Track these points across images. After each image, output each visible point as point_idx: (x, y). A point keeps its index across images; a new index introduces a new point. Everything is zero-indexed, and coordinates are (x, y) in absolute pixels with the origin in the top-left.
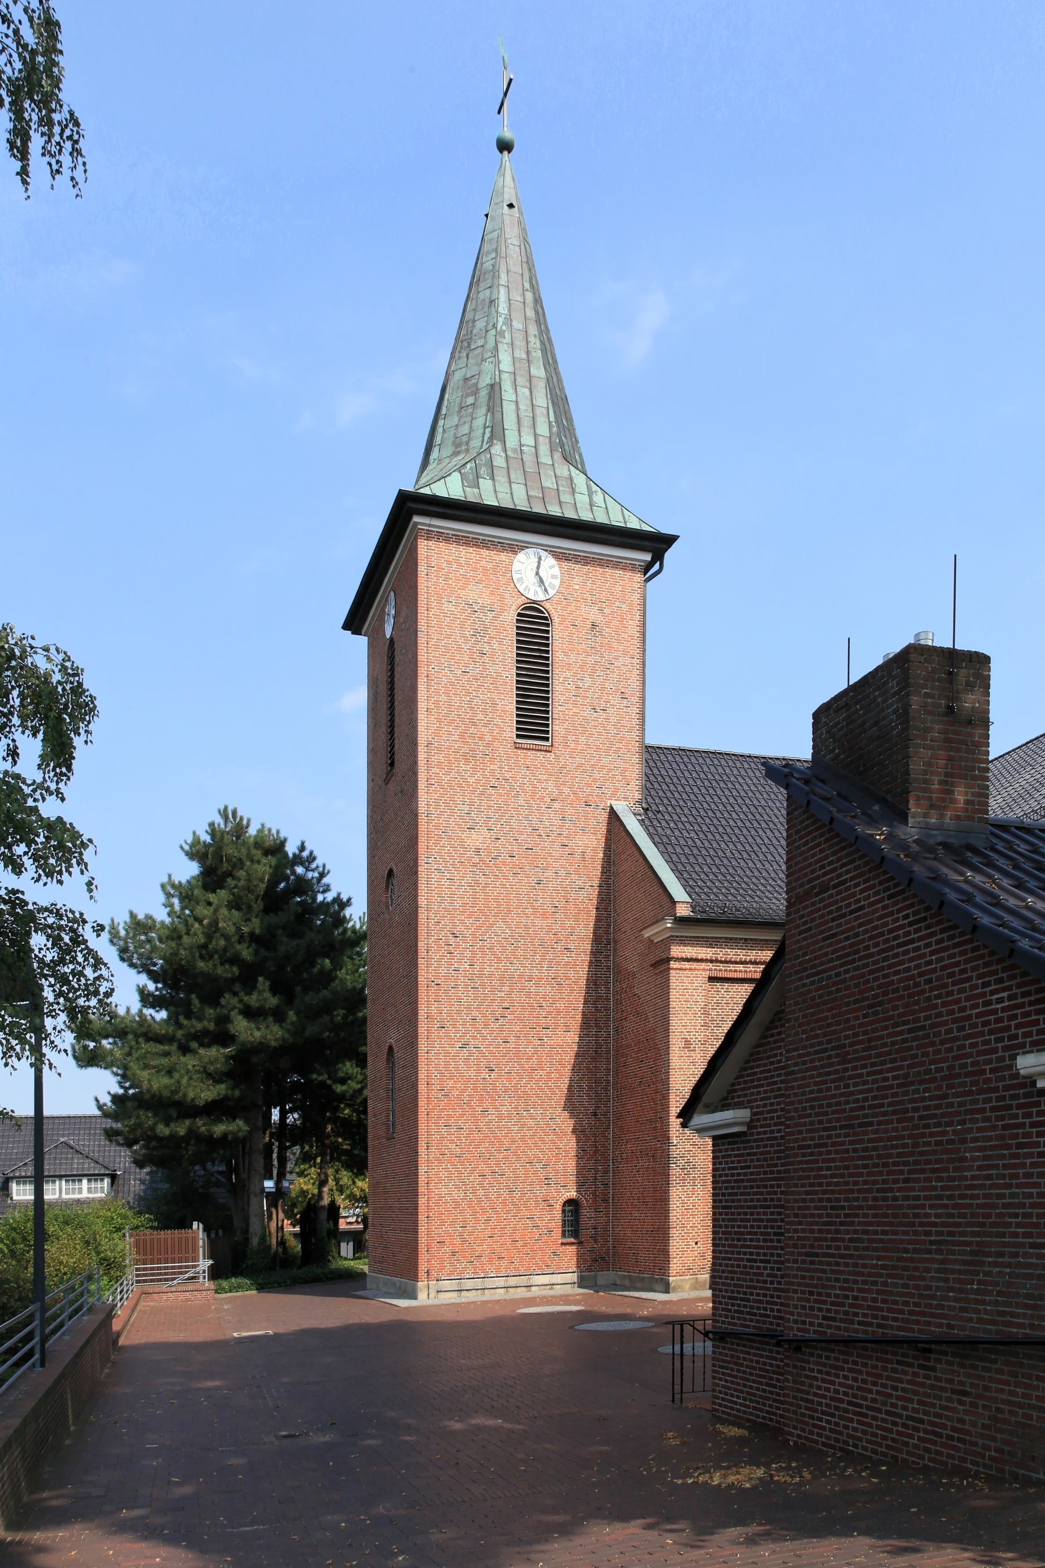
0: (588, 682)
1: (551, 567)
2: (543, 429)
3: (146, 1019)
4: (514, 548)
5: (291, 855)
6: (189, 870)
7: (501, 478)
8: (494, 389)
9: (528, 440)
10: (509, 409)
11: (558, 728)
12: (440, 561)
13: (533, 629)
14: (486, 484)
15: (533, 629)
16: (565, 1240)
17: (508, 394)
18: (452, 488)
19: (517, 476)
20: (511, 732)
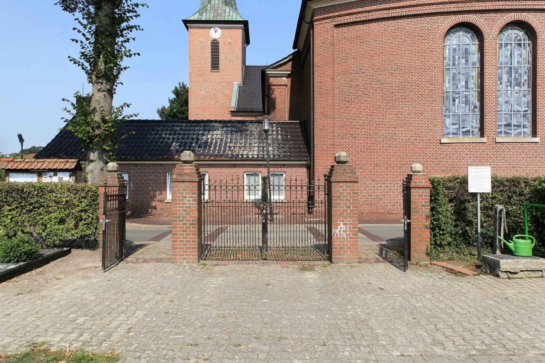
0: (228, 55)
1: (219, 31)
4: (210, 28)
6: (173, 96)
7: (208, 12)
11: (221, 67)
13: (215, 46)
15: (215, 46)
16: (421, 199)
19: (212, 11)
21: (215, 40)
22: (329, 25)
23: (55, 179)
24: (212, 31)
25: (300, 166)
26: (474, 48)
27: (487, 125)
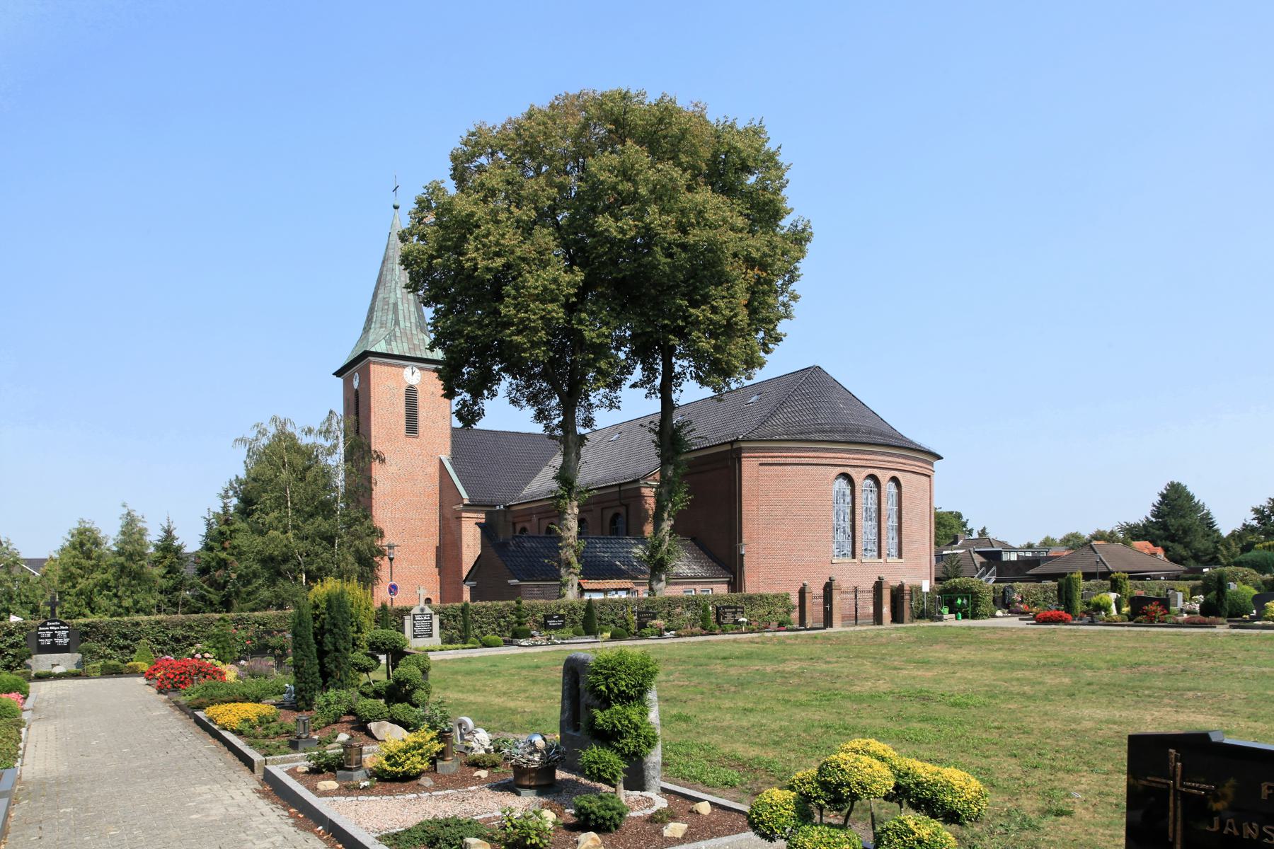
2: (413, 320)
3: (632, 351)
4: (404, 366)
5: (1255, 523)
8: (395, 305)
9: (408, 324)
10: (401, 312)
11: (421, 430)
12: (380, 374)
14: (394, 343)
17: (400, 307)
18: (381, 347)
20: (404, 432)
21: (411, 386)
22: (755, 462)
23: (616, 596)
24: (408, 371)
25: (723, 583)
26: (848, 492)
27: (858, 550)
